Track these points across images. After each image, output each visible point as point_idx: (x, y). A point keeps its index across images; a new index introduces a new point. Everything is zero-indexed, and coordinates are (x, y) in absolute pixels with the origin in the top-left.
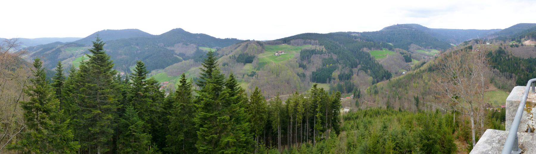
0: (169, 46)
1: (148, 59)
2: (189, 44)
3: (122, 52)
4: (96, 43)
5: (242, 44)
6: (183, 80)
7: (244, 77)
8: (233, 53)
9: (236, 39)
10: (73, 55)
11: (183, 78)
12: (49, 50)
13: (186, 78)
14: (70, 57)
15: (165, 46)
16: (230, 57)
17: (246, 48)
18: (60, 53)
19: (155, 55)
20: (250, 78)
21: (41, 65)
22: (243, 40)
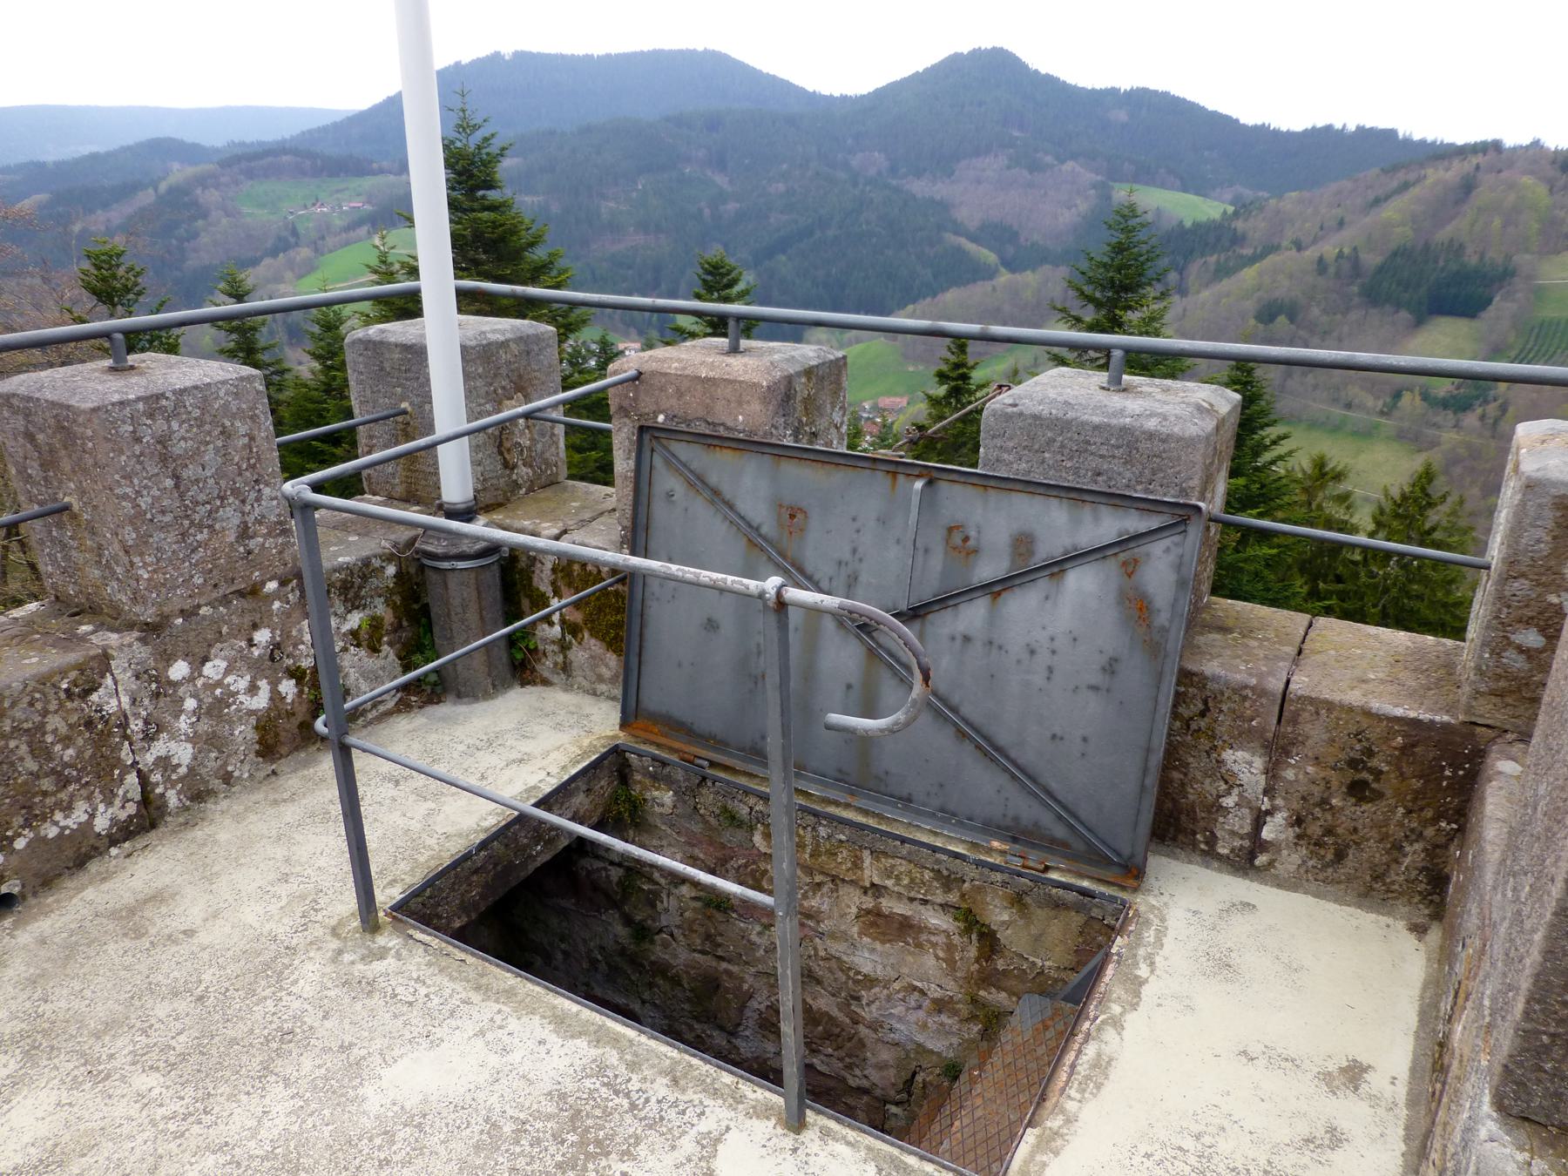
0: (919, 174)
1: (783, 258)
2: (1049, 159)
3: (622, 208)
4: (458, 144)
5: (1430, 171)
6: (957, 366)
7: (1394, 406)
8: (1347, 233)
9: (1392, 133)
10: (295, 233)
11: (953, 359)
12: (105, 206)
13: (971, 363)
14: (274, 253)
15: (893, 170)
16: (1321, 260)
17: (1457, 203)
18: (200, 223)
19: (831, 233)
20: (1438, 419)
21: (136, 284)
22: (1448, 140)
